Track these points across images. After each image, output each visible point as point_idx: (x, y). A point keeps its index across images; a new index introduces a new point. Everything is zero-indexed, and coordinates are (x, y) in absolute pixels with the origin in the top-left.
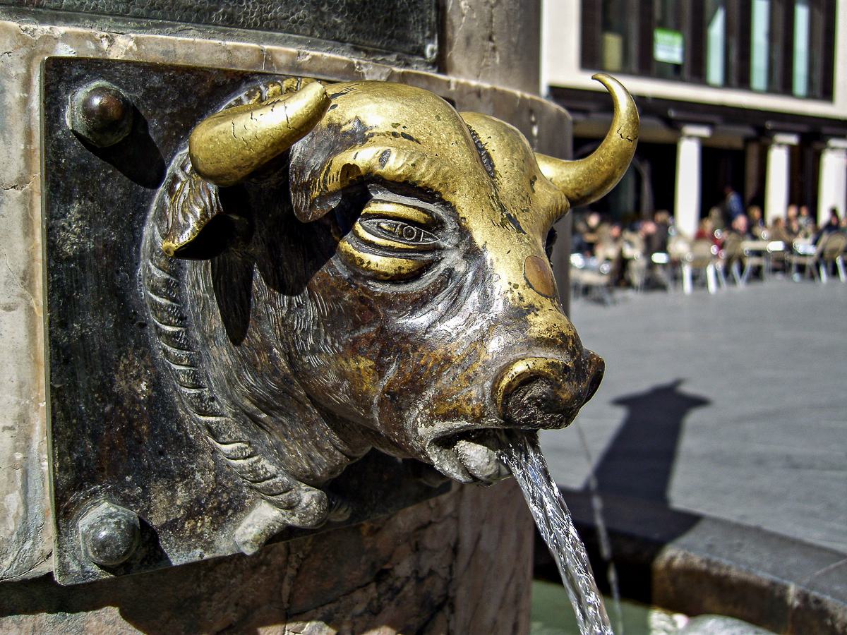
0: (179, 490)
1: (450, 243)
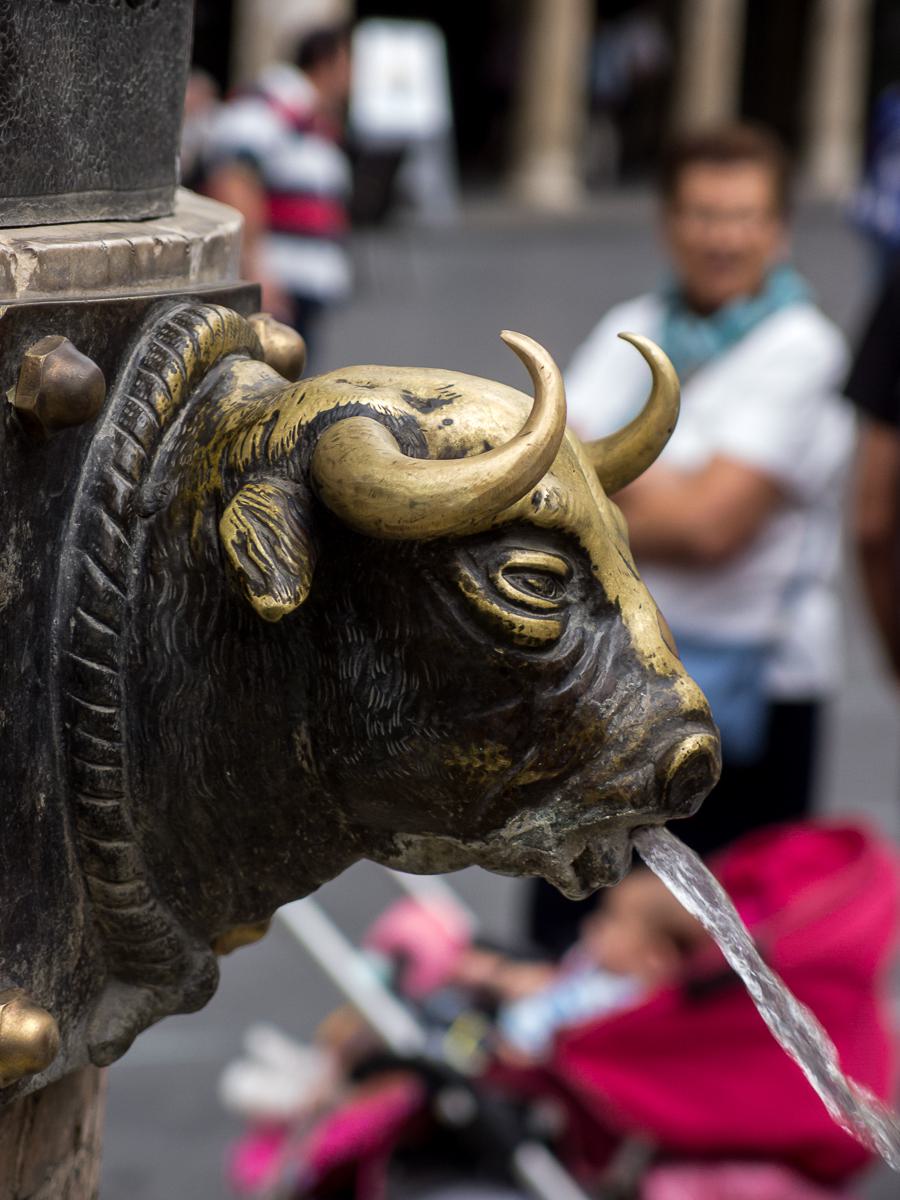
1: (575, 597)
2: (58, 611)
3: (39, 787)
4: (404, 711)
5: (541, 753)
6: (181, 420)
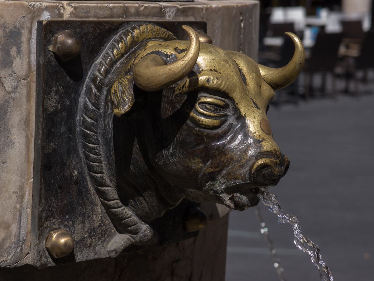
0: (86, 223)
1: (231, 113)
2: (78, 115)
3: (74, 168)
4: (173, 148)
5: (212, 162)
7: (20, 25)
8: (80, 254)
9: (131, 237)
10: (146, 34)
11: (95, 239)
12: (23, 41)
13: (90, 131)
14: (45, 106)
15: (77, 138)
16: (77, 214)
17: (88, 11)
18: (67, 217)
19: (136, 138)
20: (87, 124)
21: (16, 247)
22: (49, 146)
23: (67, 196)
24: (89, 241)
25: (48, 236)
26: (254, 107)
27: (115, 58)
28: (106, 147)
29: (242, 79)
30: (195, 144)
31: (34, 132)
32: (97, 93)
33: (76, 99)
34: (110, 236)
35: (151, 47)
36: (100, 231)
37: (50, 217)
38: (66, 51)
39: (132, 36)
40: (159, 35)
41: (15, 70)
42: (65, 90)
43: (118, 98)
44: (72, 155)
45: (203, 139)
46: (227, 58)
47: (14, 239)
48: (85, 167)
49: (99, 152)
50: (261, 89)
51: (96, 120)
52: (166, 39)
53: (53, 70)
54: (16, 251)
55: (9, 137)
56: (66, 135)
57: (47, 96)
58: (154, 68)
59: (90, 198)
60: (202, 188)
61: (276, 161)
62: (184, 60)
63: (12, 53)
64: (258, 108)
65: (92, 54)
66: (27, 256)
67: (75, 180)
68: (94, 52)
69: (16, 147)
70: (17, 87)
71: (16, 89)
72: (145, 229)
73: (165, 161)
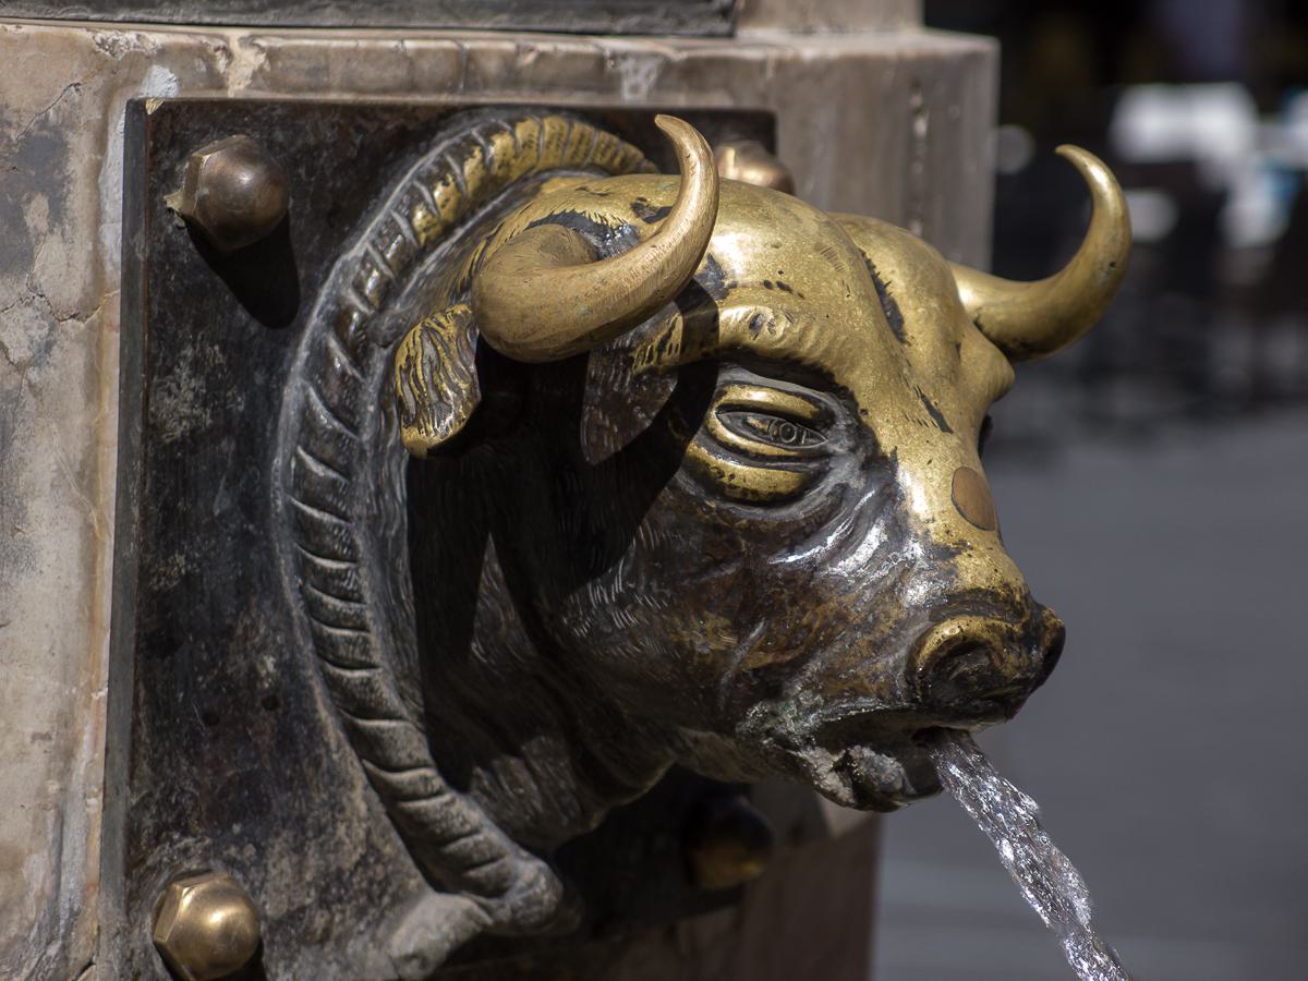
1: (841, 446)
2: (280, 450)
3: (263, 648)
5: (769, 630)
6: (454, 239)
7: (61, 114)
8: (287, 968)
9: (482, 906)
10: (537, 150)
11: (343, 912)
12: (73, 176)
13: (322, 508)
14: (153, 415)
15: (274, 536)
16: (276, 817)
17: (320, 64)
18: (237, 828)
19: (490, 537)
20: (310, 483)
21: (44, 941)
22: (167, 564)
23: (235, 751)
24: (320, 921)
25: (163, 900)
26: (930, 424)
27: (418, 241)
28: (383, 569)
29: (888, 318)
30: (703, 560)
31: (113, 513)
32: (351, 371)
33: (273, 390)
34: (403, 900)
35: (552, 197)
36: (364, 885)
37: (168, 829)
38: (229, 210)
39: (483, 160)
40: (586, 155)
41: (42, 280)
42: (230, 358)
43: (419, 387)
44: (254, 600)
45: (734, 543)
46: (827, 241)
47: (38, 911)
48: (306, 644)
49: (355, 588)
50: (959, 356)
51: (343, 471)
52: (609, 171)
53: (183, 284)
54: (45, 953)
55: (19, 530)
56: (232, 526)
57: (159, 377)
58: (546, 276)
59: (325, 760)
60: (733, 727)
61: (1010, 625)
62: (659, 244)
63: (33, 220)
64: (945, 428)
65: (332, 226)
66: (84, 975)
67: (267, 691)
68: (342, 218)
69: (44, 569)
70: (48, 346)
71: (46, 352)
72: (530, 875)
73: (596, 623)
